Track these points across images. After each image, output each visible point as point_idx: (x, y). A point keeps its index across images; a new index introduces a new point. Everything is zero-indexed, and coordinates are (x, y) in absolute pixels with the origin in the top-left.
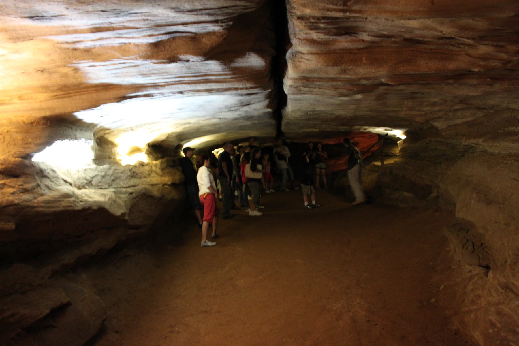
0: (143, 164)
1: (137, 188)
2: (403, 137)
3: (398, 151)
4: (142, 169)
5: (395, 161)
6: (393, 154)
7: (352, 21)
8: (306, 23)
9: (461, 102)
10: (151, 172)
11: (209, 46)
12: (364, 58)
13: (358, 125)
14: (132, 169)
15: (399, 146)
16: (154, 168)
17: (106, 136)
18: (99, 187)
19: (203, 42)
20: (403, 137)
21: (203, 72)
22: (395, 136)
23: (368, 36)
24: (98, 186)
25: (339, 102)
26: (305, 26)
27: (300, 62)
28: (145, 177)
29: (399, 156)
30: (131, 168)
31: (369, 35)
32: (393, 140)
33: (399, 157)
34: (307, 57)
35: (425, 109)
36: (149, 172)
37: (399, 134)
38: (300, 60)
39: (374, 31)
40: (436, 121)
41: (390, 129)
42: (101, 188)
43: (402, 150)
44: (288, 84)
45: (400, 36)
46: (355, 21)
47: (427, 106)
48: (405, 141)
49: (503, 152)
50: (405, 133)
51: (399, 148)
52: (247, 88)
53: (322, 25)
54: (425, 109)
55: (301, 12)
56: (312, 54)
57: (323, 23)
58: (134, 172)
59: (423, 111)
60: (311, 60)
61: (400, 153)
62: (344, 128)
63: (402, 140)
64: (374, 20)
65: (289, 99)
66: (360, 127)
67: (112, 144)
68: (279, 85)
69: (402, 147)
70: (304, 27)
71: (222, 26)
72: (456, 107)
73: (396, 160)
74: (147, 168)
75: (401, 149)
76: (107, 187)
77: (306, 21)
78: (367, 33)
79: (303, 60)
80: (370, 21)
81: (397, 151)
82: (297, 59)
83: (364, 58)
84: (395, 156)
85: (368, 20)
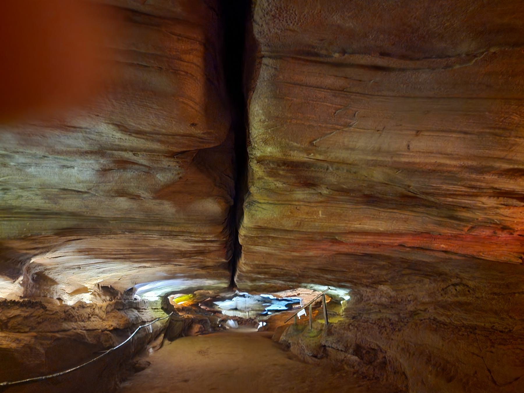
0: (84, 306)
1: (68, 333)
2: (347, 298)
3: (341, 311)
4: (82, 311)
5: (339, 321)
6: (336, 313)
7: (312, 171)
8: (265, 168)
9: (409, 268)
10: (92, 315)
11: (162, 184)
12: (320, 212)
13: (305, 283)
14: (68, 311)
15: (342, 306)
16: (97, 311)
17: (46, 273)
18: (17, 331)
19: (157, 178)
20: (347, 298)
21: (184, 247)
22: (338, 295)
23: (326, 189)
24: (15, 329)
25: (291, 258)
26: (264, 171)
27: (256, 211)
28: (83, 321)
29: (343, 315)
30: (67, 308)
31: (327, 188)
32: (335, 301)
33: (343, 316)
34: (264, 206)
35: (372, 272)
36: (89, 315)
37: (343, 294)
38: (257, 209)
39: (334, 185)
40: (381, 284)
41: (334, 288)
42: (19, 332)
43: (346, 310)
44: (236, 279)
45: (360, 191)
46: (316, 171)
47: (375, 268)
48: (348, 301)
49: (456, 322)
50: (349, 294)
51: (343, 308)
52: (200, 233)
53: (281, 172)
54: (372, 272)
55: (261, 152)
56: (268, 203)
57: (283, 170)
58: (69, 315)
59: (369, 274)
60: (267, 210)
61: (344, 313)
62: (292, 284)
63: (345, 301)
64: (335, 172)
65: (243, 251)
66: (307, 284)
67: (54, 282)
68: (235, 234)
69: (345, 307)
70: (263, 173)
71: (178, 162)
72: (404, 272)
73: (340, 319)
74: (89, 310)
75: (345, 309)
76: (27, 330)
77: (266, 166)
78: (326, 186)
79: (259, 209)
80: (332, 173)
81: (341, 310)
82: (253, 207)
83: (320, 212)
84: (339, 315)
85: (329, 171)
